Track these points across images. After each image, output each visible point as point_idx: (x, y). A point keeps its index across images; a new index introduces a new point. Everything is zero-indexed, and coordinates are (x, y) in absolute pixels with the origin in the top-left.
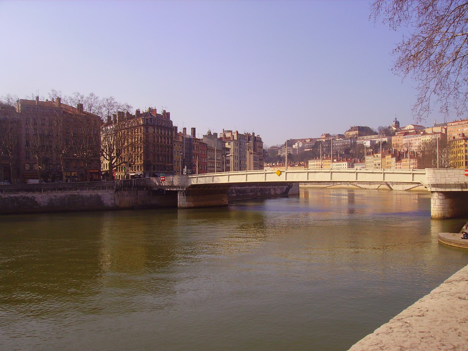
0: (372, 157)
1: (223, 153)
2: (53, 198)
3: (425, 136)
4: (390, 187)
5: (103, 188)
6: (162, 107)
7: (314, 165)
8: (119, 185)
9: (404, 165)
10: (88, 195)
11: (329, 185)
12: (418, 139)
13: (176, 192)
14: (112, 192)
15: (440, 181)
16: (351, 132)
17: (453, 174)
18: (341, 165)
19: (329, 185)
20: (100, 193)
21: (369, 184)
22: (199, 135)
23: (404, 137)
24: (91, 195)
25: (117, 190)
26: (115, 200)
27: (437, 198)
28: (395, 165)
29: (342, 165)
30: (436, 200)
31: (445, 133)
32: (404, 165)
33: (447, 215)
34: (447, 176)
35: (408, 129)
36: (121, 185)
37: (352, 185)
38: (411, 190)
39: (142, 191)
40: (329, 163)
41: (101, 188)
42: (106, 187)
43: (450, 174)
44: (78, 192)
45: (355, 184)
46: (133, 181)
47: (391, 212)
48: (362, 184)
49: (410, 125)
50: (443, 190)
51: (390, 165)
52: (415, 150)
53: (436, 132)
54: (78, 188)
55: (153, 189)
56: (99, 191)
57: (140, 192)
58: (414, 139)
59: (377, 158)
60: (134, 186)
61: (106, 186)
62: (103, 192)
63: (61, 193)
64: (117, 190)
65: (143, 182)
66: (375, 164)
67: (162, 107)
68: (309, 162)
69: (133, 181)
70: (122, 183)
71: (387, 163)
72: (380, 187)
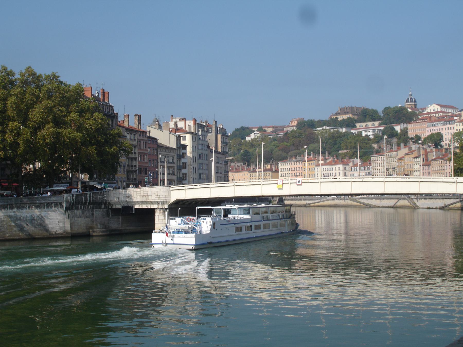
1: (177, 153)
6: (97, 83)
8: (71, 201)
10: (28, 215)
11: (313, 202)
12: (451, 128)
13: (152, 211)
18: (332, 170)
19: (313, 202)
21: (379, 199)
22: (312, 120)
23: (428, 124)
26: (64, 223)
35: (432, 111)
36: (72, 202)
38: (448, 208)
39: (99, 210)
40: (313, 166)
41: (46, 206)
44: (14, 212)
46: (88, 196)
47: (329, 248)
49: (434, 105)
54: (14, 205)
55: (114, 207)
56: (43, 210)
57: (96, 211)
60: (89, 203)
61: (52, 203)
64: (67, 209)
65: (100, 197)
67: (97, 83)
68: (280, 164)
69: (88, 196)
70: (74, 197)
72: (398, 204)
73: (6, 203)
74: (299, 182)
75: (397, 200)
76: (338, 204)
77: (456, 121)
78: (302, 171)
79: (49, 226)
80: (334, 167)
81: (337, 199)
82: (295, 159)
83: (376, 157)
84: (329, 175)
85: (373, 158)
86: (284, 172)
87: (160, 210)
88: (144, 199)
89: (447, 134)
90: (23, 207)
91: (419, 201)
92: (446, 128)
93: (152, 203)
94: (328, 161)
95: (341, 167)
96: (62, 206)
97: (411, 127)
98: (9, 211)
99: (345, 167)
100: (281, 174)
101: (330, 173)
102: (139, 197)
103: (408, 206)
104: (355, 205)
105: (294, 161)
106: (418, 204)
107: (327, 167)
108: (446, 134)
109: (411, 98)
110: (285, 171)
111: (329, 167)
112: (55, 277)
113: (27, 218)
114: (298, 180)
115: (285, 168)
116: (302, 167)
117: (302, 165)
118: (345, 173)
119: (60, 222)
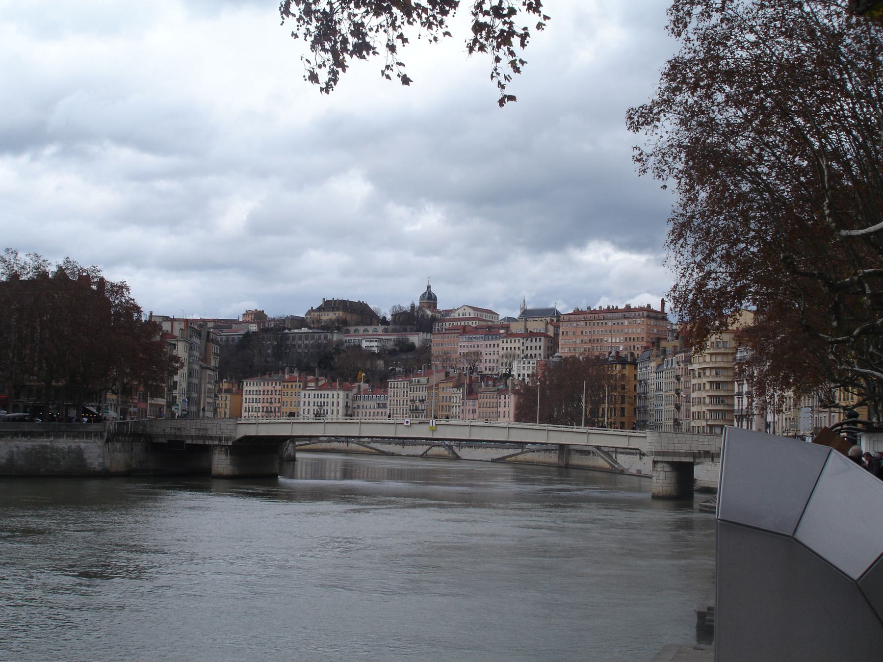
0: (406, 383)
2: (15, 449)
3: (513, 340)
4: (454, 453)
5: (88, 435)
7: (258, 392)
9: (482, 406)
12: (490, 345)
14: (100, 443)
15: (666, 448)
16: (323, 313)
17: (684, 439)
18: (327, 398)
20: (82, 443)
21: (400, 444)
24: (70, 447)
25: (108, 441)
27: (661, 469)
28: (461, 404)
29: (329, 397)
30: (661, 473)
31: (553, 336)
32: (482, 406)
33: (673, 493)
34: (676, 441)
35: (461, 316)
37: (359, 443)
40: (297, 390)
42: (93, 434)
43: (680, 439)
44: (50, 441)
45: (364, 442)
48: (385, 443)
50: (670, 459)
51: (448, 404)
52: (486, 369)
53: (534, 331)
55: (155, 441)
58: (484, 343)
59: (418, 386)
61: (91, 432)
62: (87, 442)
63: (26, 441)
64: (108, 441)
66: (412, 398)
68: (245, 383)
71: (441, 398)
72: (430, 452)
73: (42, 430)
74: (407, 422)
75: (427, 447)
76: (336, 448)
77: (502, 335)
78: (280, 397)
79: (88, 461)
80: (330, 393)
81: (335, 441)
82: (270, 376)
83: (396, 383)
84: (322, 404)
85: (391, 384)
86: (251, 397)
87: (221, 448)
88: (202, 433)
89: (488, 354)
90: (61, 436)
91: (461, 449)
92: (487, 345)
93: (211, 438)
94: (320, 383)
95: (342, 394)
96: (102, 437)
97: (435, 339)
98: (45, 440)
99: (347, 395)
100: (246, 398)
101: (324, 402)
102: (194, 430)
103: (445, 456)
104: (363, 451)
105: (268, 380)
106: (459, 454)
107: (319, 392)
108: (486, 354)
109: (430, 294)
110: (253, 394)
111: (323, 392)
112: (447, 545)
113: (65, 450)
114: (406, 420)
115: (253, 390)
116: (280, 391)
117: (281, 387)
118: (347, 403)
119: (99, 456)
